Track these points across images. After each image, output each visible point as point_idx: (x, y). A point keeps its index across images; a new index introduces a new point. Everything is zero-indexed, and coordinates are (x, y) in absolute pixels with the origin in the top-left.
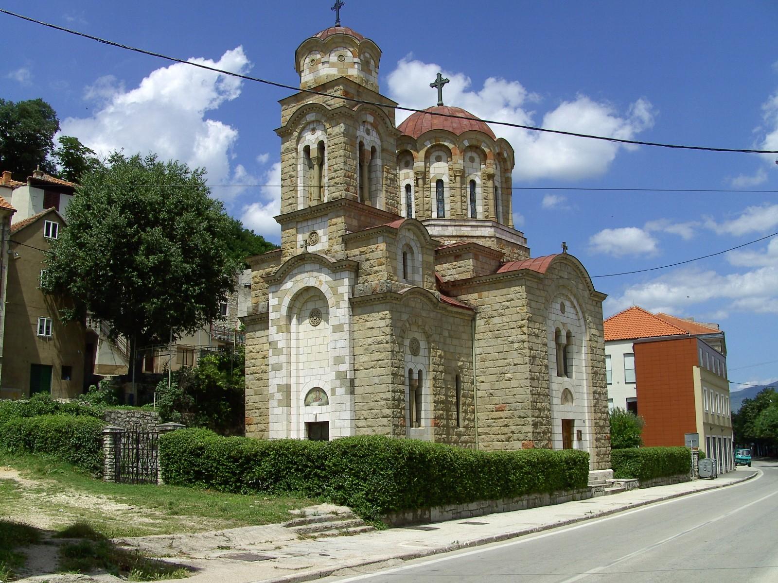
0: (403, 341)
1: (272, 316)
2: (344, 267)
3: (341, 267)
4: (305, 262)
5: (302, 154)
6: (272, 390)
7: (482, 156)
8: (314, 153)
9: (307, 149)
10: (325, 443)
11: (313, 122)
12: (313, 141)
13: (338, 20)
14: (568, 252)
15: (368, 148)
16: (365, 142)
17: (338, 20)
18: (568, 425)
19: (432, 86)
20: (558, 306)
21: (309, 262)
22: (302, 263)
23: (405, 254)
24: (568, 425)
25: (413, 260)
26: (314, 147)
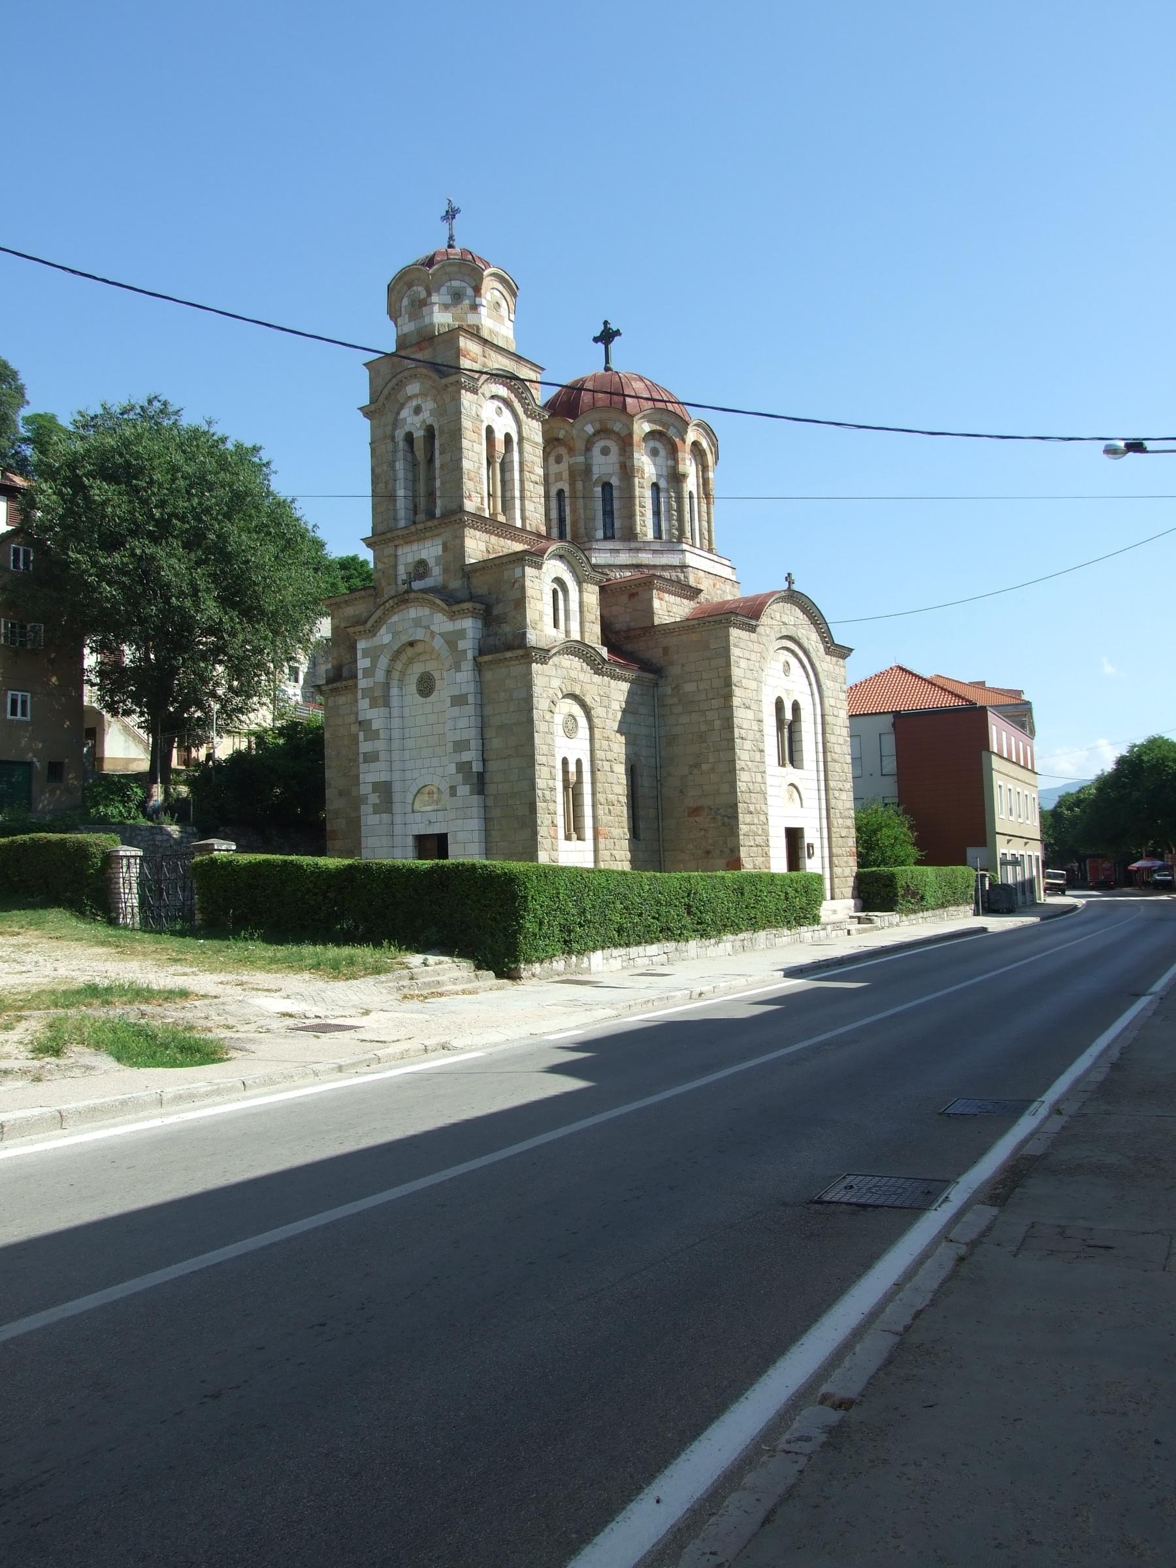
0: (552, 717)
1: (363, 683)
2: (466, 611)
3: (461, 612)
4: (408, 605)
5: (401, 445)
6: (365, 789)
7: (669, 446)
8: (419, 446)
9: (409, 438)
10: (441, 862)
11: (416, 396)
12: (418, 425)
13: (451, 238)
14: (795, 587)
15: (499, 437)
16: (494, 427)
17: (451, 238)
18: (794, 837)
19: (596, 340)
20: (780, 666)
21: (416, 604)
22: (404, 606)
23: (555, 592)
24: (794, 837)
25: (566, 600)
26: (419, 434)
